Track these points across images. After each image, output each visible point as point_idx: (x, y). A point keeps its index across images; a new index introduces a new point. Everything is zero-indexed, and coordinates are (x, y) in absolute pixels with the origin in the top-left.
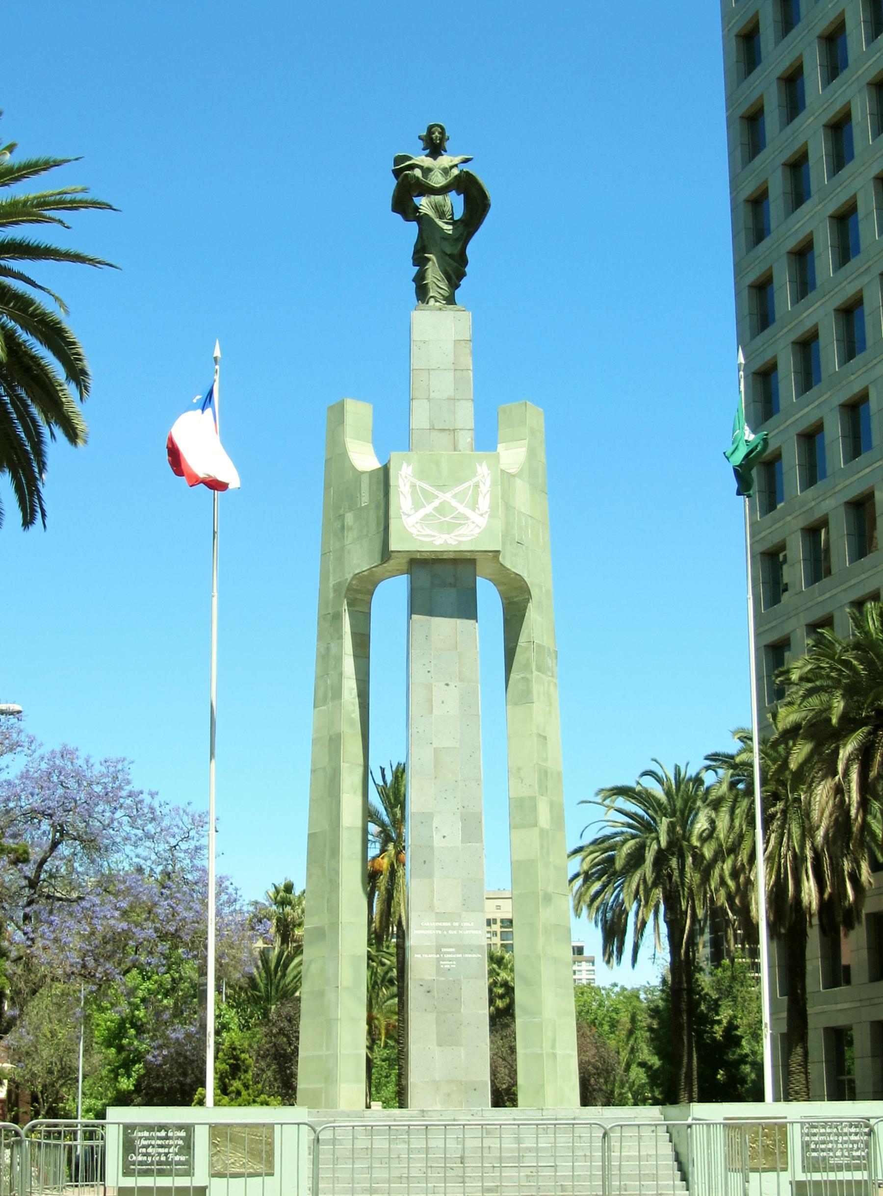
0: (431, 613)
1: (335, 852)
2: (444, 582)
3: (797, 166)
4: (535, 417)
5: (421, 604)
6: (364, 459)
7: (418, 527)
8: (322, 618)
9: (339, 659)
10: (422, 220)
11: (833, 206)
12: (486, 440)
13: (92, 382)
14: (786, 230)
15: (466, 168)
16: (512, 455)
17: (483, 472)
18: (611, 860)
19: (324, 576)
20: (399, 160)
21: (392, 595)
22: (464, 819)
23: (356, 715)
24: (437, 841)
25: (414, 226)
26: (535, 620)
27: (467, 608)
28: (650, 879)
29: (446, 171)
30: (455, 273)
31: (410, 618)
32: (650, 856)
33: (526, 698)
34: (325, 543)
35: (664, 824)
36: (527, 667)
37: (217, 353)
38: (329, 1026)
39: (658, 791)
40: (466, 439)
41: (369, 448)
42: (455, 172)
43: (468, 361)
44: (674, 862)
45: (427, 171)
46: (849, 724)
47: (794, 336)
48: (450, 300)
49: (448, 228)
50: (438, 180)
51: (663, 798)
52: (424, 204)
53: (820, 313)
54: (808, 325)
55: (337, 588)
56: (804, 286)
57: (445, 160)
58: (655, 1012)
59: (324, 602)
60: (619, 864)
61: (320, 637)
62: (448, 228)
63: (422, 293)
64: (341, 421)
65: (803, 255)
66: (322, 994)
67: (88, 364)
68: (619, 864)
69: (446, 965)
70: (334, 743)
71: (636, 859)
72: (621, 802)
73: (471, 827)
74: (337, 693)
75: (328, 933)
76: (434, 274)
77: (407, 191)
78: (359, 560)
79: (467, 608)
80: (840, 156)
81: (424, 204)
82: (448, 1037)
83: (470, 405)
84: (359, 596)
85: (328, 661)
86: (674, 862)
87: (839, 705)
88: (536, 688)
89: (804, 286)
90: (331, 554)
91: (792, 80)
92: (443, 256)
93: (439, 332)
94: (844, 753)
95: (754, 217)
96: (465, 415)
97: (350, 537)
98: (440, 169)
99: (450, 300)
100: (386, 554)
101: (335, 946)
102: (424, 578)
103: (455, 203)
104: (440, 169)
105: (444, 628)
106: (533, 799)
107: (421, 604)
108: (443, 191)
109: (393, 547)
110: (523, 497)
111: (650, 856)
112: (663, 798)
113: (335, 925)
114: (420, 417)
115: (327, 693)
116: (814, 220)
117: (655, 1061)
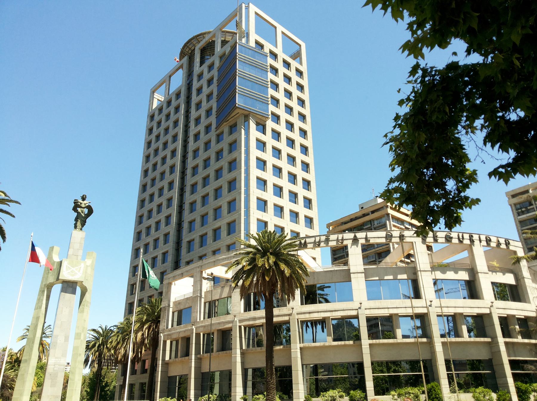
0: (66, 292)
1: (33, 342)
2: (69, 286)
3: (150, 212)
4: (95, 255)
5: (64, 290)
6: (56, 259)
7: (66, 275)
8: (40, 291)
9: (42, 300)
10: (78, 213)
11: (156, 220)
12: (83, 259)
13: (7, 240)
14: (146, 223)
15: (90, 204)
16: (89, 262)
17: (82, 265)
18: (89, 345)
19: (42, 282)
20: (75, 200)
21: (57, 288)
22: (65, 337)
23: (44, 313)
24: (58, 341)
25: (76, 214)
26: (87, 295)
27: (74, 292)
28: (96, 349)
29: (85, 204)
30: (83, 224)
31: (60, 293)
32: (97, 345)
33: (83, 312)
34: (44, 275)
35: (101, 338)
36: (84, 305)
37: (32, 235)
38: (24, 382)
39: (101, 331)
40: (80, 258)
41: (57, 256)
42: (87, 205)
43: (83, 242)
44: (102, 347)
45: (81, 203)
46: (147, 321)
47: (145, 243)
48: (81, 229)
49: (83, 215)
50: (83, 206)
51: (102, 333)
52: (79, 210)
53: (150, 240)
54: (148, 241)
55: (45, 285)
56: (148, 234)
57: (85, 202)
58: (90, 379)
59: (41, 287)
60: (90, 347)
61: (39, 295)
62: (83, 215)
63: (76, 227)
64: (53, 250)
65: (148, 228)
66: (23, 375)
67: (6, 236)
68: (90, 347)
69: (55, 369)
70: (38, 318)
71: (94, 346)
72: (92, 333)
73: (67, 339)
74: (40, 307)
75: (28, 361)
76: (79, 224)
77: (76, 206)
78: (51, 279)
79: (74, 292)
80: (159, 211)
81: (79, 210)
82: (53, 385)
83: (82, 251)
84: (49, 287)
85: (39, 300)
86: (102, 347)
87: (145, 317)
88: (85, 310)
89: (148, 234)
90: (45, 277)
91: (152, 196)
92: (81, 220)
93: (78, 235)
94: (145, 327)
95: (140, 219)
96: (80, 253)
97: (50, 274)
98: (84, 203)
99: (81, 229)
100: (58, 279)
101: (29, 364)
102: (65, 285)
103: (86, 211)
104: (84, 203)
105: (68, 296)
106: (80, 333)
107: (64, 290)
108: (84, 208)
109: (60, 278)
110: (89, 270)
111: (97, 345)
112: (102, 333)
113: (30, 359)
114: (71, 252)
115: (38, 307)
116: (152, 222)
117: (89, 390)
